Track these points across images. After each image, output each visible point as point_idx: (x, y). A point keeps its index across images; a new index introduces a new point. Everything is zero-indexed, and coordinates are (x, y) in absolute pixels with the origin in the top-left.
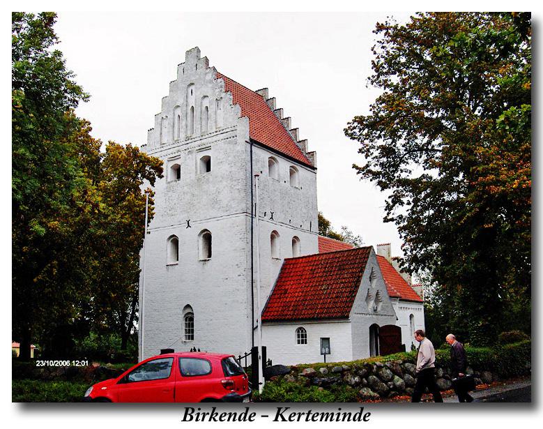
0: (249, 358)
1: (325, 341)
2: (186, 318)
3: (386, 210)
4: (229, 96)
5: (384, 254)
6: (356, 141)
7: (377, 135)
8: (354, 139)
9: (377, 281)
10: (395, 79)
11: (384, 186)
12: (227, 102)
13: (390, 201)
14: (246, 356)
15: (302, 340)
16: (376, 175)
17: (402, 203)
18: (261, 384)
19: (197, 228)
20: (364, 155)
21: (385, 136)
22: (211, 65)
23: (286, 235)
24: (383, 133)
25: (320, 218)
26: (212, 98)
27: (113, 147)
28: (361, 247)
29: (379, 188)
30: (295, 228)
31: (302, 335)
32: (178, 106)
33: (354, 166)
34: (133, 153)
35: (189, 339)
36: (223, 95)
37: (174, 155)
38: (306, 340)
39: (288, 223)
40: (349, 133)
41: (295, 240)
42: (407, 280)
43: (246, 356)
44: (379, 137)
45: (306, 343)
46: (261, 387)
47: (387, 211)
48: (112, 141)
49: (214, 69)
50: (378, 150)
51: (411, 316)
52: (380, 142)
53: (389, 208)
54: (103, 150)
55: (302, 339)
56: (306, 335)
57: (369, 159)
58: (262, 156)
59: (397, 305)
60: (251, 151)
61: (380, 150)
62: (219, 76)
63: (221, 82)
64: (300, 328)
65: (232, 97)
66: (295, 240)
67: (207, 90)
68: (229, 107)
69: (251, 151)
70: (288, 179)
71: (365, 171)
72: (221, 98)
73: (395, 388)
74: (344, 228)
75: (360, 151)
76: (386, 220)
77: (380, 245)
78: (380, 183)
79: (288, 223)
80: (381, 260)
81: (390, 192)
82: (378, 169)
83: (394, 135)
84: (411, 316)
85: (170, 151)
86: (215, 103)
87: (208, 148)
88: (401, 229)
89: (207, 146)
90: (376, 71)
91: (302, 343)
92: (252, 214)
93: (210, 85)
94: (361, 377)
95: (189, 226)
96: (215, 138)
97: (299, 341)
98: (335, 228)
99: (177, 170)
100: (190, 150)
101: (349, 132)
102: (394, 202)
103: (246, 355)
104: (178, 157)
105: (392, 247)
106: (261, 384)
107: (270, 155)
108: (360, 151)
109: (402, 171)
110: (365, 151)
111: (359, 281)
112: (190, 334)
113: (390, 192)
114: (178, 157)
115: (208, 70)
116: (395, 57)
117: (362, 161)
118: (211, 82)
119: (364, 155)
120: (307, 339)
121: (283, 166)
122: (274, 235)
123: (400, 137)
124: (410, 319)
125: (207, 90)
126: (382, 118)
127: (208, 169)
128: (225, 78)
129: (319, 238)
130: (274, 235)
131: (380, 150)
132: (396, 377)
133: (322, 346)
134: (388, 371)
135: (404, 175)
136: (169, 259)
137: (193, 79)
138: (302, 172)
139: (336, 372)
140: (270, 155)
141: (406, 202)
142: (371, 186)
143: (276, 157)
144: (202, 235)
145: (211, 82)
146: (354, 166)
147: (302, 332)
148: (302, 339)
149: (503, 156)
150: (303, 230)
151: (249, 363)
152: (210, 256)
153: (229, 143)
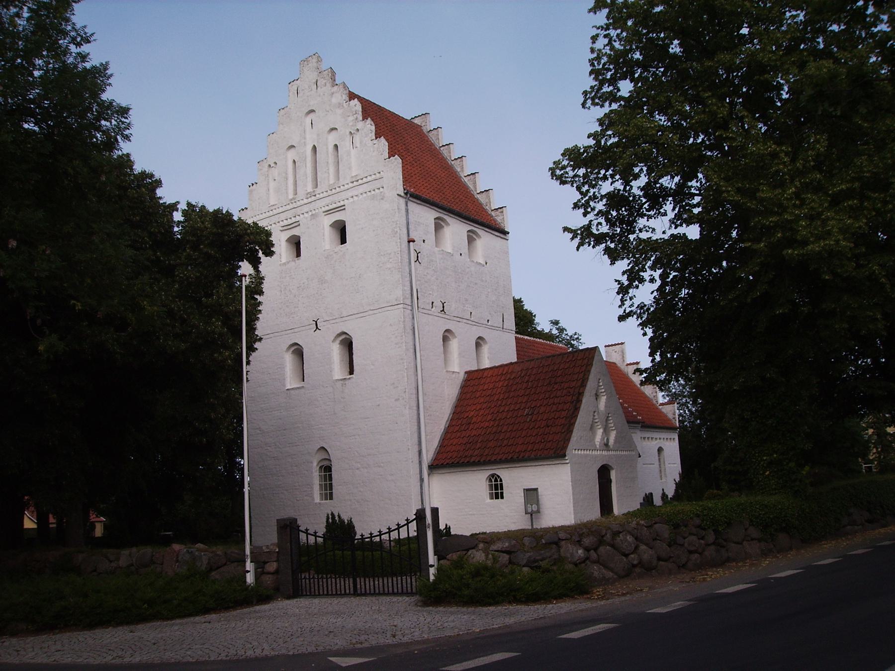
0: (413, 526)
1: (531, 494)
2: (321, 467)
3: (618, 293)
4: (369, 126)
5: (615, 358)
6: (568, 186)
7: (601, 176)
8: (563, 183)
9: (616, 472)
10: (626, 87)
11: (613, 256)
12: (367, 136)
13: (624, 280)
14: (407, 524)
15: (497, 494)
16: (599, 239)
17: (642, 280)
18: (432, 566)
19: (329, 331)
20: (582, 211)
21: (612, 176)
22: (338, 81)
23: (464, 336)
24: (610, 172)
25: (518, 304)
26: (344, 131)
27: (191, 211)
28: (581, 348)
29: (606, 259)
30: (477, 324)
31: (496, 486)
32: (293, 146)
33: (566, 229)
34: (222, 219)
35: (326, 499)
36: (360, 125)
37: (290, 222)
38: (502, 493)
39: (468, 317)
40: (558, 174)
41: (479, 342)
42: (651, 396)
43: (407, 524)
44: (605, 178)
45: (502, 498)
46: (432, 571)
47: (621, 295)
48: (572, 206)
49: (345, 86)
50: (601, 200)
51: (660, 450)
52: (606, 187)
53: (623, 290)
54: (178, 216)
55: (497, 490)
56: (501, 485)
57: (591, 216)
58: (425, 216)
59: (637, 436)
60: (407, 211)
61: (605, 200)
62: (352, 96)
63: (356, 105)
64: (493, 475)
65: (373, 128)
66: (479, 342)
67: (335, 119)
68: (371, 143)
69: (407, 211)
70: (465, 250)
71: (585, 236)
72: (358, 130)
73: (641, 564)
74: (556, 323)
75: (576, 206)
76: (622, 318)
77: (609, 346)
78: (607, 251)
79: (468, 317)
80: (611, 367)
81: (623, 264)
82: (605, 229)
83: (628, 177)
84: (660, 450)
85: (283, 216)
86: (348, 139)
87: (342, 208)
88: (643, 325)
89: (339, 204)
90: (596, 79)
91: (497, 498)
92: (412, 306)
93: (339, 111)
94: (587, 550)
95: (317, 328)
96: (349, 193)
97: (491, 494)
98: (543, 324)
99: (296, 244)
100: (314, 212)
101: (558, 172)
102: (631, 280)
103: (408, 522)
104: (297, 224)
105: (627, 348)
106: (432, 566)
107: (438, 215)
108: (576, 206)
109: (640, 230)
110: (583, 206)
111: (579, 401)
112: (328, 491)
113: (623, 264)
114: (297, 224)
115: (336, 87)
116: (625, 52)
117: (578, 220)
118: (340, 105)
119: (582, 211)
120: (504, 491)
121: (456, 230)
122: (447, 336)
123: (637, 177)
124: (659, 454)
125: (335, 119)
126: (608, 149)
127: (343, 241)
128: (361, 100)
129: (516, 337)
130: (447, 336)
131: (605, 200)
132: (643, 547)
133: (527, 501)
134: (630, 538)
135: (644, 236)
136: (288, 380)
137: (313, 104)
138: (486, 240)
139: (549, 544)
140: (438, 215)
141: (648, 278)
142: (594, 255)
143: (445, 217)
144: (338, 341)
145: (340, 105)
146: (566, 229)
147: (496, 480)
148: (497, 490)
149: (803, 202)
150: (492, 328)
151: (413, 534)
152: (351, 372)
153: (373, 198)
